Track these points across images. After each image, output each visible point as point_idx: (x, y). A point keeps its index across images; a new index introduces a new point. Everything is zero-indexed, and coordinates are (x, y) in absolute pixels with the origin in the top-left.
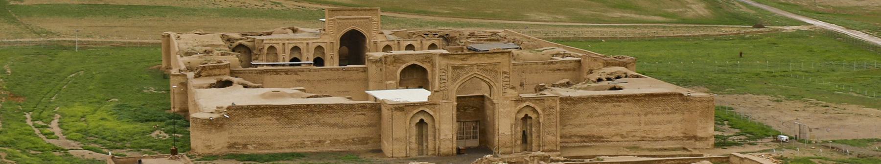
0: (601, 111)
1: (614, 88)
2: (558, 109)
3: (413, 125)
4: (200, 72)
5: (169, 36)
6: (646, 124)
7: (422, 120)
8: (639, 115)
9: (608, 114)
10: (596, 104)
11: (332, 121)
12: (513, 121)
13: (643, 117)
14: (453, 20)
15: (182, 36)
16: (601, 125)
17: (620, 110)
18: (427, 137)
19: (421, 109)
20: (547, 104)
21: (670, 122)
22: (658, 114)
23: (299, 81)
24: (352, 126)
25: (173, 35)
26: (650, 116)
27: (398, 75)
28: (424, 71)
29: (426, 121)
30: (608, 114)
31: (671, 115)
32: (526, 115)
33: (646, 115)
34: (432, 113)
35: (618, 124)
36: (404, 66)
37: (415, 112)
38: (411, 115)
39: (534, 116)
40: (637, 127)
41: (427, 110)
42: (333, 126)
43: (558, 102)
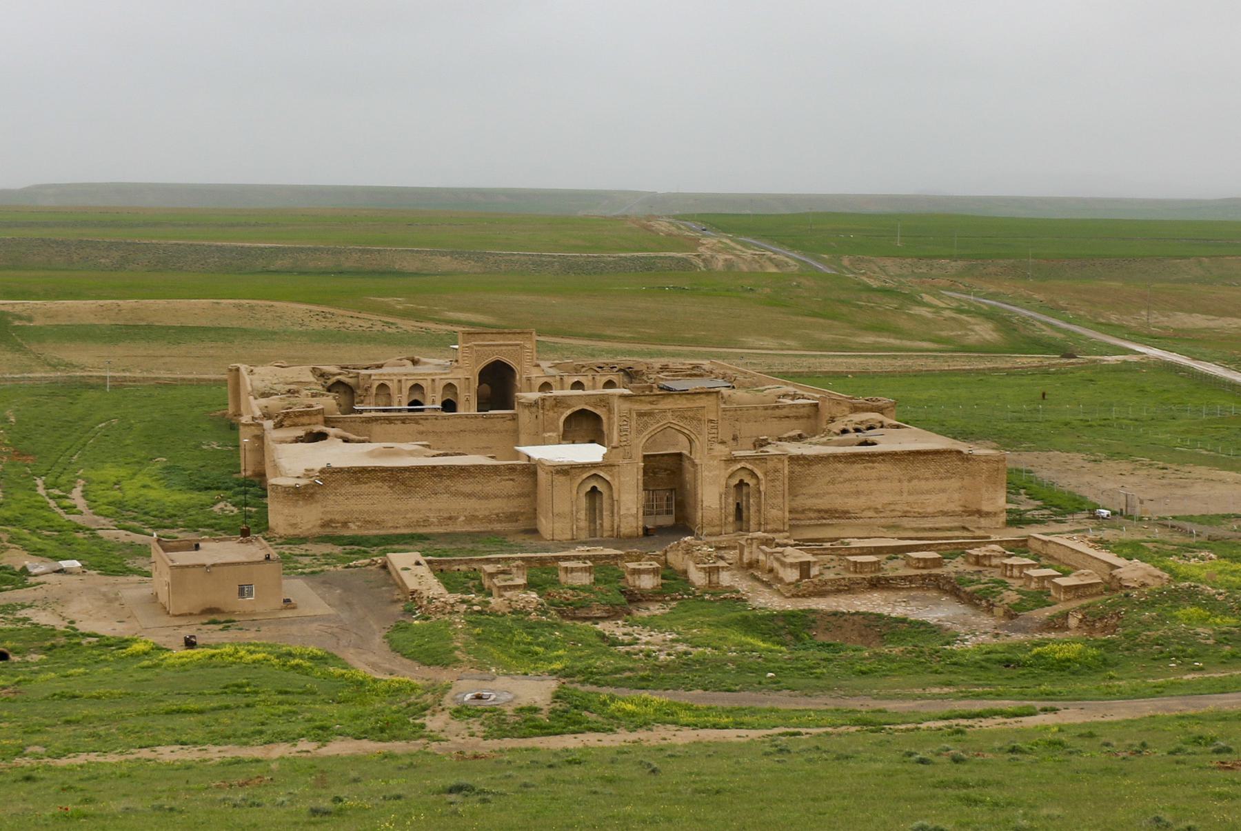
1: (865, 443)
3: (582, 494)
5: (238, 370)
7: (594, 489)
8: (900, 481)
9: (857, 479)
10: (840, 466)
11: (468, 488)
12: (723, 490)
13: (906, 483)
15: (256, 370)
16: (847, 496)
17: (874, 474)
18: (601, 511)
19: (593, 472)
20: (770, 465)
21: (943, 491)
22: (927, 479)
23: (422, 433)
25: (244, 368)
26: (915, 482)
28: (597, 418)
29: (600, 489)
30: (857, 479)
31: (945, 482)
32: (741, 481)
33: (910, 481)
34: (608, 478)
36: (569, 412)
37: (585, 476)
39: (752, 482)
40: (898, 498)
41: (602, 474)
42: (469, 496)
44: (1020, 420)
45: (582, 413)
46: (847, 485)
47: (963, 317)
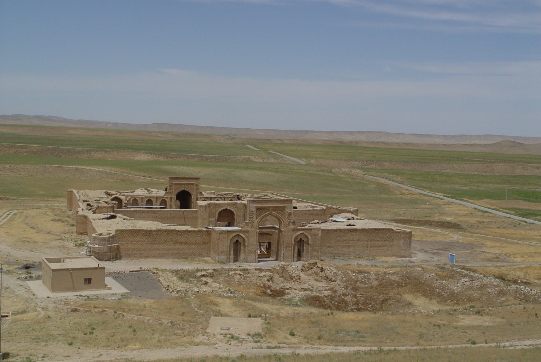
0: (344, 238)
1: (350, 225)
2: (320, 235)
4: (95, 211)
5: (72, 191)
6: (371, 247)
7: (237, 241)
8: (367, 241)
9: (349, 240)
13: (369, 242)
14: (411, 148)
15: (80, 191)
19: (237, 233)
20: (313, 232)
23: (156, 217)
24: (193, 244)
25: (75, 191)
26: (373, 242)
27: (217, 216)
28: (232, 213)
30: (349, 240)
32: (301, 239)
33: (371, 241)
35: (354, 246)
36: (220, 210)
38: (231, 237)
41: (241, 234)
42: (181, 243)
43: (320, 232)
44: (360, 272)
45: (226, 210)
46: (344, 242)
47: (18, 316)
